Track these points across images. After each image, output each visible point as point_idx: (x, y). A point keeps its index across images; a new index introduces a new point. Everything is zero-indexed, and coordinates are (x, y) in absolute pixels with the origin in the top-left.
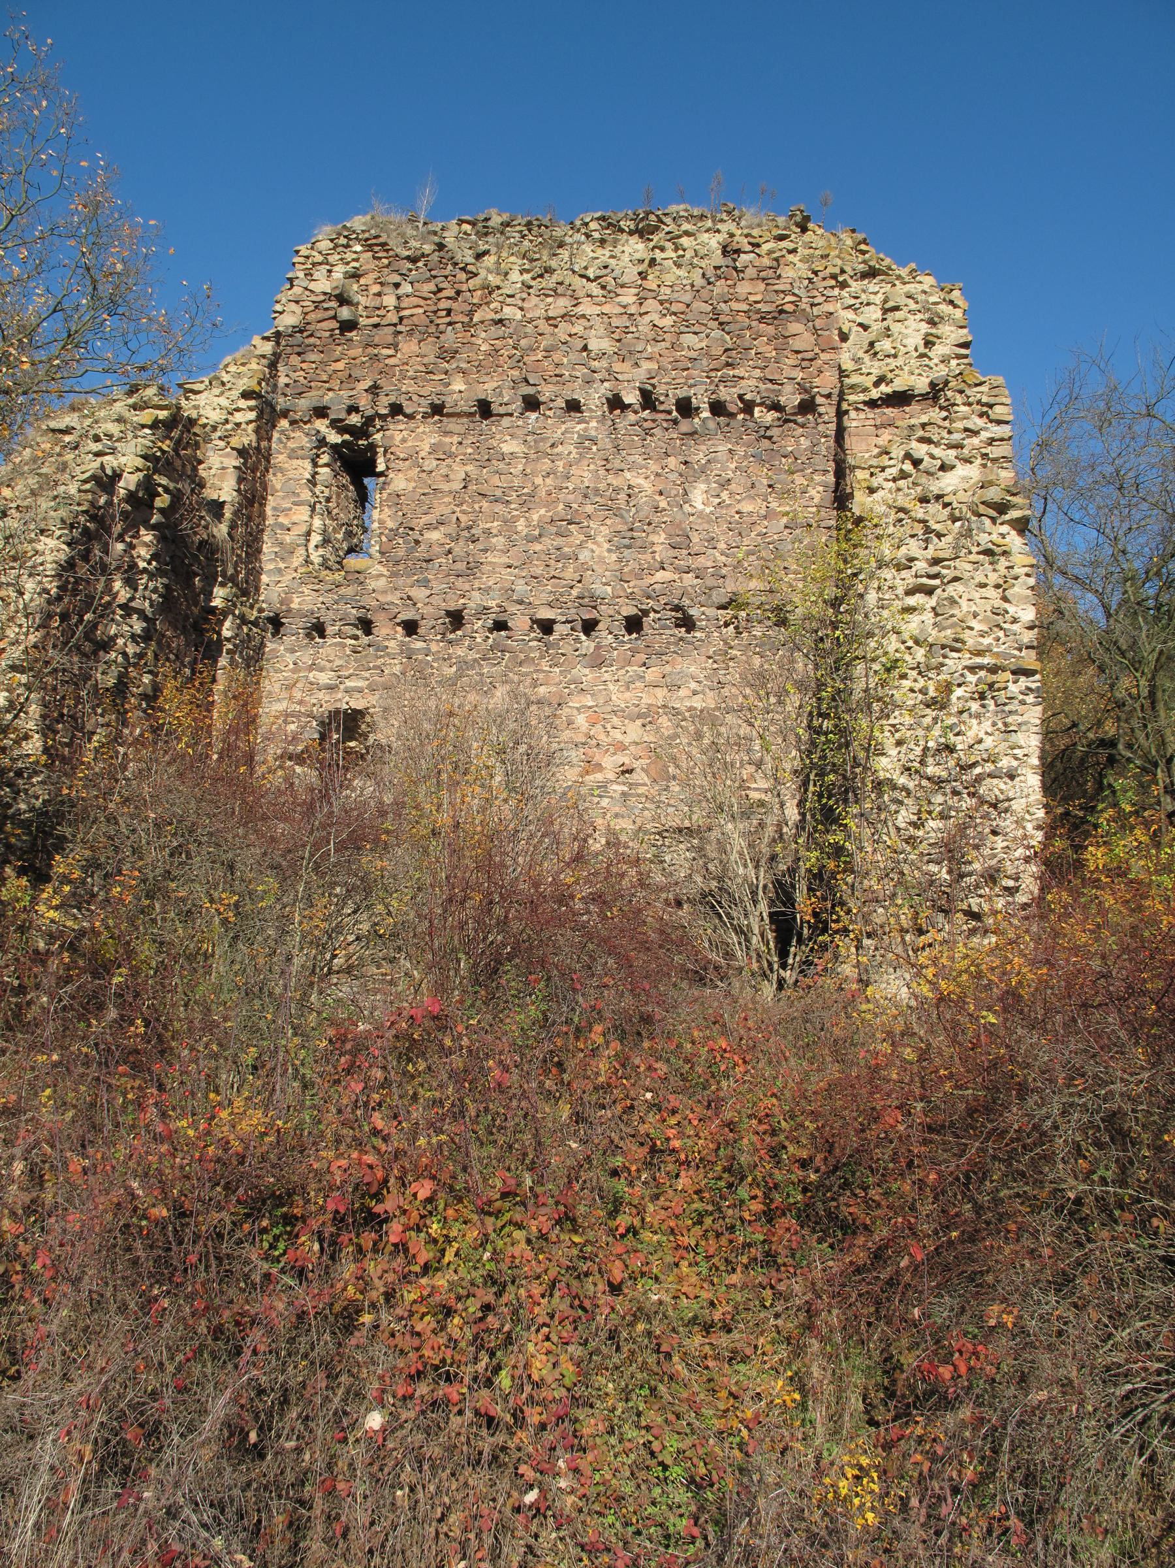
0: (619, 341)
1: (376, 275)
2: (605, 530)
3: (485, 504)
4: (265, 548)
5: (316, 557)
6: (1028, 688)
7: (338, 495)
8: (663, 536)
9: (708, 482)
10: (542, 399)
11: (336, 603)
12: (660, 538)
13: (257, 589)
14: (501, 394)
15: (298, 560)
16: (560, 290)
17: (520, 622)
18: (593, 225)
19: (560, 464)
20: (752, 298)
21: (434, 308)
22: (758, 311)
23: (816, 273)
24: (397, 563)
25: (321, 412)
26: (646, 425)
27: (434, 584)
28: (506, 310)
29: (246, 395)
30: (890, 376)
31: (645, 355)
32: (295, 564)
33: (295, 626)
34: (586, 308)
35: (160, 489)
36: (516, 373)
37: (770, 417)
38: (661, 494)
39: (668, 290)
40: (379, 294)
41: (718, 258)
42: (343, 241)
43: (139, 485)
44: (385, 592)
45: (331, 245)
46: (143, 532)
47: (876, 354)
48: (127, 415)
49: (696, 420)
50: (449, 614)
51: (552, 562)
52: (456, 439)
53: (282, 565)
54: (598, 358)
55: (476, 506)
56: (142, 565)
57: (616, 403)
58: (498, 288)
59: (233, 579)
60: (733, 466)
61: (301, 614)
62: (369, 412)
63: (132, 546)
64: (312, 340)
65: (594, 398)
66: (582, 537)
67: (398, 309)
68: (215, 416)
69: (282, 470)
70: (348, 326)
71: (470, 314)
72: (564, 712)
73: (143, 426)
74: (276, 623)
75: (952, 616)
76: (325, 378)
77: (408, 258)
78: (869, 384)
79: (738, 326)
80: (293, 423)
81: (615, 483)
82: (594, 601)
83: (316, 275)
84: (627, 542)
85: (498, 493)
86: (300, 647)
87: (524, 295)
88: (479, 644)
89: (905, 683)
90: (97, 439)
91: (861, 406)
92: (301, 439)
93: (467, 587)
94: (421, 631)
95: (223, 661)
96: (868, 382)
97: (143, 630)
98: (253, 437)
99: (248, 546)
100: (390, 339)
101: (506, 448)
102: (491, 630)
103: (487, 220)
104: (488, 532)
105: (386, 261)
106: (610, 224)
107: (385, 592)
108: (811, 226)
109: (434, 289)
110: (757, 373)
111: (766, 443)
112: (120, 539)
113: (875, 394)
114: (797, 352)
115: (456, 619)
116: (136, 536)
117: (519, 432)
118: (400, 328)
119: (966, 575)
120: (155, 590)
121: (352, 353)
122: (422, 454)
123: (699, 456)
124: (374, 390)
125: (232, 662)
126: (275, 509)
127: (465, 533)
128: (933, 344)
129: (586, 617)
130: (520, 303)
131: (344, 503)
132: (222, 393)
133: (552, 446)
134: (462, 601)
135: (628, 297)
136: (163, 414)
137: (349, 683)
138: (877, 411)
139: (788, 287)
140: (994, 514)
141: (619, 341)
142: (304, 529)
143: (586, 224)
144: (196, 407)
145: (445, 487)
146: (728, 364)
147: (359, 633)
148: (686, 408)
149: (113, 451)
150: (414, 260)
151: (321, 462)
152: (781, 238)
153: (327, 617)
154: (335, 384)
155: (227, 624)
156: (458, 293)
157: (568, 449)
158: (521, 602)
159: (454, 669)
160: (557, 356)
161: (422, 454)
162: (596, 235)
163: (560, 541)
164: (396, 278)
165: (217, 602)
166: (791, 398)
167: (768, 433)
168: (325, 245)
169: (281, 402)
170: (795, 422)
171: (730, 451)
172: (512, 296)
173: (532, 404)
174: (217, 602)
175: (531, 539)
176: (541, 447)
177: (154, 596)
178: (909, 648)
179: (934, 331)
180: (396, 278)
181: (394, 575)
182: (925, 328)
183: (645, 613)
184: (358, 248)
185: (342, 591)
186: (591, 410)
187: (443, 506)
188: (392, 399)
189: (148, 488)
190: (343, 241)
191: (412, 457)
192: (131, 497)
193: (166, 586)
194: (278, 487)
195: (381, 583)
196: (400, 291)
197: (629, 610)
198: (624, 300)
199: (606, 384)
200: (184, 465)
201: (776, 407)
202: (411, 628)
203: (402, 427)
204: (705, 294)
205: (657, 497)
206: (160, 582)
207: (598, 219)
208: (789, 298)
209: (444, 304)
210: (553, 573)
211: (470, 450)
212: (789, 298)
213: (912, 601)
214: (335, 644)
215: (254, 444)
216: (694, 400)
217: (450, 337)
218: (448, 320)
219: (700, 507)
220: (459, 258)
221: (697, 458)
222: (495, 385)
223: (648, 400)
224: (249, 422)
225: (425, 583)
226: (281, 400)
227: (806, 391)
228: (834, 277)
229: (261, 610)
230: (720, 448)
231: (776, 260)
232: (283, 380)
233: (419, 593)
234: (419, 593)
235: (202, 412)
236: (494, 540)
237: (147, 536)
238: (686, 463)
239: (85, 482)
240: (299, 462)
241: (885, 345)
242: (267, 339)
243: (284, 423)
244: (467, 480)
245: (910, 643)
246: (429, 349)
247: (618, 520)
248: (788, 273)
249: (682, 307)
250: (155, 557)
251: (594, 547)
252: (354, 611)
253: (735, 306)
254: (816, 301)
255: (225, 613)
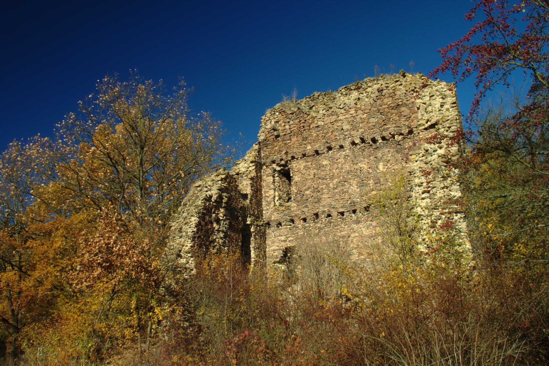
0: (352, 125)
1: (283, 120)
2: (355, 182)
3: (320, 181)
4: (263, 203)
5: (277, 204)
6: (461, 217)
7: (282, 184)
8: (372, 181)
9: (383, 162)
10: (332, 147)
11: (284, 216)
12: (371, 181)
13: (262, 216)
14: (321, 148)
15: (272, 205)
16: (333, 113)
17: (334, 213)
18: (343, 90)
19: (340, 165)
20: (389, 103)
21: (299, 127)
22: (391, 107)
23: (407, 91)
24: (299, 202)
25: (273, 162)
26: (363, 148)
27: (309, 206)
28: (319, 123)
29: (252, 162)
30: (430, 119)
31: (360, 127)
32: (272, 207)
33: (273, 224)
34: (341, 117)
35: (224, 197)
36: (324, 140)
37: (400, 137)
38: (370, 168)
39: (363, 107)
40: (284, 126)
41: (377, 94)
42: (273, 113)
43: (217, 198)
44: (296, 211)
45: (270, 114)
46: (221, 209)
47: (427, 112)
48: (214, 178)
49: (378, 143)
50: (314, 214)
51: (341, 194)
52: (310, 163)
53: (268, 208)
54: (346, 131)
55: (318, 182)
56: (221, 218)
57: (353, 143)
58: (316, 117)
59: (253, 215)
60: (390, 155)
61: (274, 221)
62: (286, 160)
63: (218, 214)
64: (269, 142)
65: (347, 144)
66: (349, 185)
67: (290, 129)
68: (243, 170)
69: (265, 181)
70: (277, 136)
71: (309, 126)
72: (350, 239)
73: (219, 181)
74: (268, 224)
75: (435, 199)
76: (273, 152)
77: (291, 114)
78: (424, 123)
79: (386, 113)
80: (267, 166)
81: (356, 167)
82: (353, 203)
83: (267, 124)
84: (362, 184)
85: (324, 177)
86: (275, 230)
87: (323, 117)
88: (324, 222)
89: (423, 221)
90: (206, 187)
91: (423, 130)
92: (269, 171)
93: (318, 206)
94: (307, 221)
95: (252, 239)
96: (424, 122)
97: (224, 236)
98: (255, 173)
99: (257, 204)
100: (289, 138)
101: (324, 163)
102: (327, 217)
103: (314, 96)
104: (322, 189)
105: (285, 116)
106: (348, 89)
107: (296, 211)
108: (406, 74)
109: (299, 121)
110: (394, 125)
111: (399, 146)
112: (214, 213)
113: (427, 125)
114: (405, 116)
115: (317, 215)
116: (219, 210)
117: (327, 158)
118: (291, 134)
119: (438, 186)
120: (226, 224)
121: (280, 144)
122: (302, 169)
123: (379, 155)
124: (286, 153)
125: (256, 239)
126: (264, 192)
127: (316, 190)
128: (443, 105)
129: (353, 209)
130: (322, 120)
131: (284, 186)
132: (246, 163)
133: (337, 160)
134: (317, 210)
135: (352, 112)
136: (223, 176)
137: (289, 239)
138: (428, 131)
139: (399, 97)
140: (445, 164)
141: (352, 125)
142: (273, 196)
143: (341, 91)
144: (239, 168)
145: (309, 178)
146: (384, 125)
147: (291, 224)
148: (374, 141)
149: (210, 190)
150: (292, 114)
151: (276, 176)
152: (397, 81)
153: (282, 221)
154: (276, 153)
155: (252, 228)
156: (305, 121)
157: (342, 160)
158: (334, 208)
159: (318, 230)
160: (334, 133)
161: (302, 169)
162: (344, 93)
163: (343, 188)
164: (288, 120)
165: (248, 223)
166: (405, 131)
167: (400, 143)
168: (269, 115)
169: (263, 161)
170: (407, 138)
171: (388, 151)
172: (320, 118)
173: (330, 148)
174: (248, 223)
175: (334, 189)
176: (334, 161)
177: (226, 226)
178: (423, 210)
179: (444, 101)
180: (288, 120)
181: (298, 205)
182: (441, 100)
183: (370, 205)
184: (277, 114)
185: (285, 212)
186: (347, 147)
187: (309, 183)
188: (291, 155)
189: (220, 197)
190: (273, 113)
191: (299, 171)
192: (216, 201)
193: (229, 222)
194: (265, 185)
195: (295, 208)
196: (290, 124)
197: (366, 205)
198: (351, 112)
199: (350, 139)
200: (232, 188)
201: (401, 134)
202: (305, 220)
203: (295, 162)
204: (374, 105)
205: (369, 170)
206: (227, 222)
207: (344, 88)
208: (400, 100)
209: (302, 125)
210: (342, 198)
211: (314, 166)
212: (400, 100)
213: (423, 196)
214: (285, 228)
215: (255, 175)
216: (376, 138)
217: (305, 134)
218: (304, 129)
219: (382, 170)
220: (304, 111)
221: (379, 155)
222: (319, 145)
223: (363, 140)
224: (253, 170)
225: (307, 206)
226: (263, 161)
227: (409, 127)
228: (413, 90)
229: (264, 221)
230: (385, 151)
231: (394, 90)
232: (262, 155)
233: (305, 210)
234: (305, 210)
235: (240, 169)
236: (324, 191)
237: (222, 210)
238: (376, 157)
239: (202, 200)
240: (269, 177)
241: (430, 109)
242: (257, 144)
243: (265, 167)
244: (314, 175)
245: (424, 209)
246: (300, 138)
247: (358, 178)
248: (398, 93)
249: (368, 111)
250: (224, 215)
251: (353, 188)
252: (289, 218)
253: (383, 106)
254: (408, 99)
255: (251, 225)
